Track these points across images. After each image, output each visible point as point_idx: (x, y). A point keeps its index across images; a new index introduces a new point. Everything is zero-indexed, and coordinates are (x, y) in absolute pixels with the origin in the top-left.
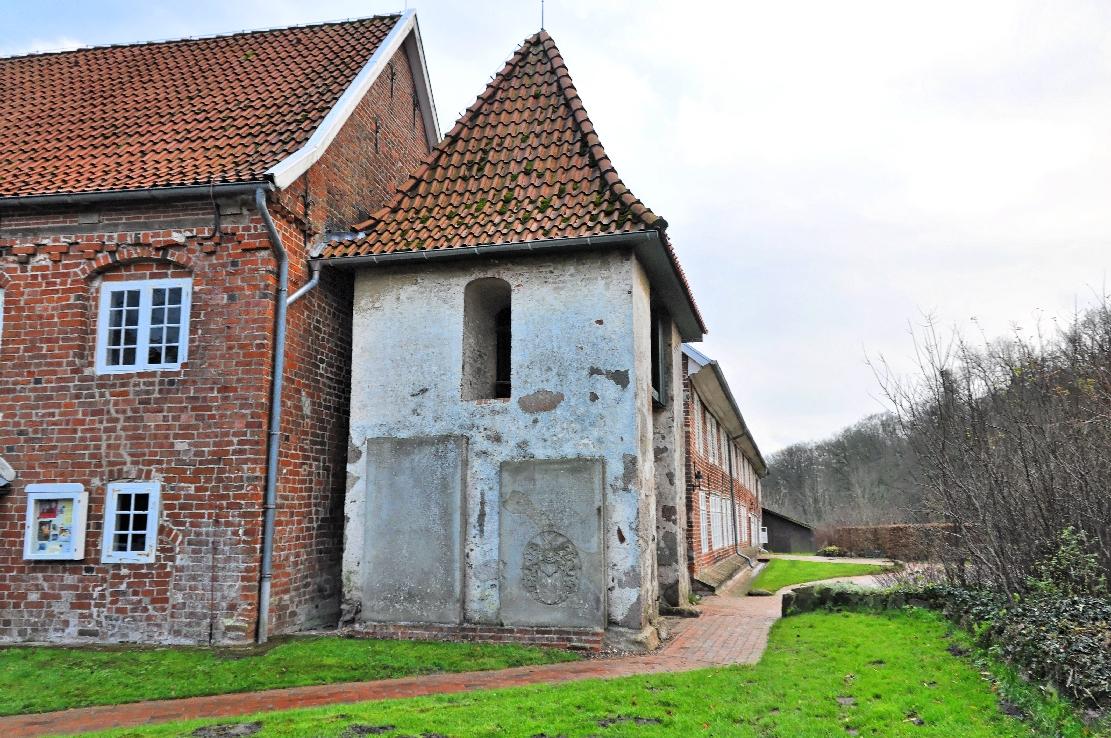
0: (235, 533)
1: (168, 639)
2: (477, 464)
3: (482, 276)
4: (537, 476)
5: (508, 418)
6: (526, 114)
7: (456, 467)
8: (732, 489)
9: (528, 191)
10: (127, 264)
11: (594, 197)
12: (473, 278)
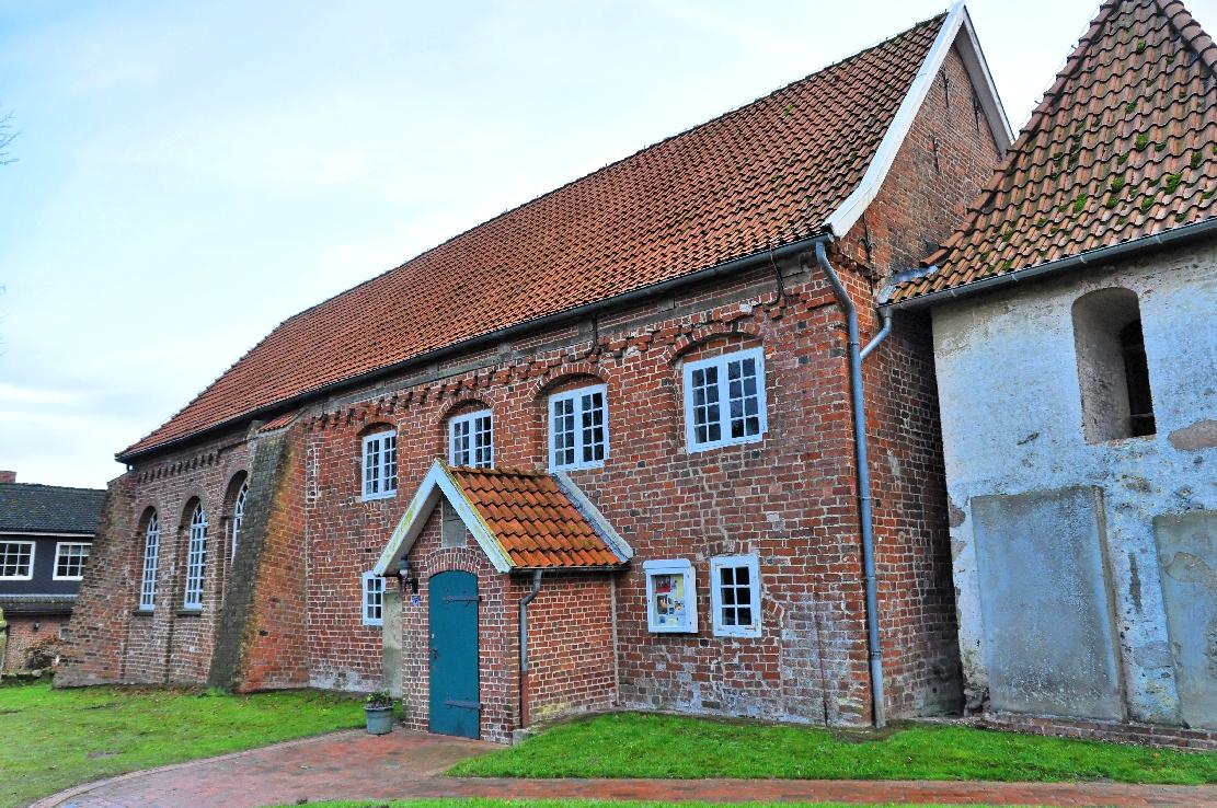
0: (837, 607)
1: (786, 717)
2: (1118, 520)
3: (1093, 287)
5: (1155, 460)
6: (1128, 78)
7: (1090, 525)
9: (1143, 171)
10: (702, 343)
12: (1081, 293)
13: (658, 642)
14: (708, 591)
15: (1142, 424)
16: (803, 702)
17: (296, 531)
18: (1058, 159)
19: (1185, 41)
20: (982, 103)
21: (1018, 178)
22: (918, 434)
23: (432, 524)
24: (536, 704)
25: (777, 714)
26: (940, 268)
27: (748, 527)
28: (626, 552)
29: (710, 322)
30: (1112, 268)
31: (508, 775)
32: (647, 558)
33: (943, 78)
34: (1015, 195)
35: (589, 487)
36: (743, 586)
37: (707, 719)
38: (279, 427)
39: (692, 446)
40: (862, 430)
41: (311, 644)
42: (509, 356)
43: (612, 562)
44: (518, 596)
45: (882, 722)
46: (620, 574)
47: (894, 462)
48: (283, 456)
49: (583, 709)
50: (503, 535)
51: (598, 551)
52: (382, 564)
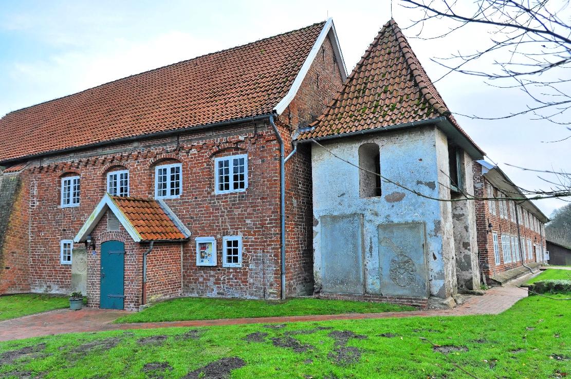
0: (271, 256)
1: (249, 297)
2: (367, 225)
3: (366, 142)
4: (394, 230)
6: (384, 63)
8: (518, 230)
9: (385, 101)
11: (416, 102)
12: (362, 144)
13: (200, 269)
14: (221, 250)
15: (378, 193)
16: (256, 291)
17: (24, 221)
18: (359, 91)
19: (403, 53)
20: (337, 59)
21: (345, 96)
22: (304, 191)
23: (103, 220)
24: (148, 295)
25: (246, 296)
26: (316, 128)
27: (239, 225)
28: (188, 233)
29: (227, 142)
30: (372, 136)
31: (140, 322)
32: (197, 237)
33: (323, 49)
34: (344, 103)
35: (173, 206)
36: (235, 248)
37: (220, 299)
38: (16, 171)
39: (217, 191)
40: (283, 189)
41: (31, 273)
42: (138, 147)
43: (182, 238)
44: (143, 251)
45: (284, 297)
46: (185, 242)
47: (295, 201)
48: (19, 185)
49: (168, 297)
50: (137, 226)
51: (176, 233)
52: (78, 238)
